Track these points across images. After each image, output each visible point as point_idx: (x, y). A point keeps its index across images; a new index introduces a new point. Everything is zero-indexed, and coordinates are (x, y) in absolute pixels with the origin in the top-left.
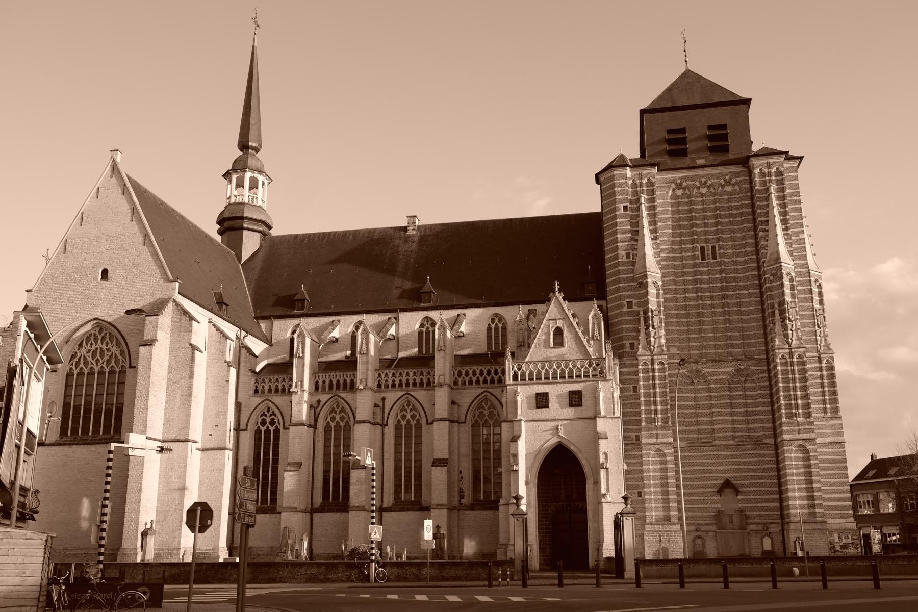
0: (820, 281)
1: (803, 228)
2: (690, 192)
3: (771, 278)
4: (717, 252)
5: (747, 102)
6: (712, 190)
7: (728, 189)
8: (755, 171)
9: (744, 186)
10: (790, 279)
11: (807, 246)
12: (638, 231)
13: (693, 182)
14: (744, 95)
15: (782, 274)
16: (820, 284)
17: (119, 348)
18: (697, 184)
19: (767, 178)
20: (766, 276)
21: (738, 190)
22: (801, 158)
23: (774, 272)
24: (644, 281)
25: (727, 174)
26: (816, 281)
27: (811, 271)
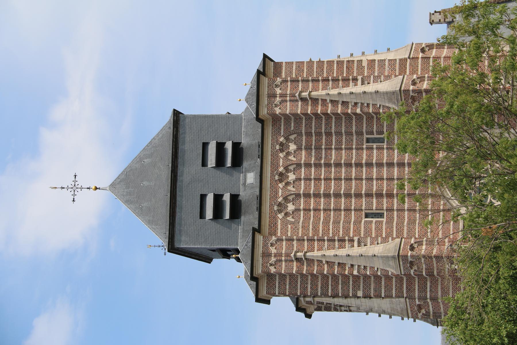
0: (423, 46)
1: (353, 61)
2: (293, 164)
3: (415, 267)
4: (375, 136)
5: (176, 114)
6: (291, 168)
7: (292, 147)
8: (272, 272)
9: (292, 129)
10: (419, 245)
11: (377, 57)
12: (339, 263)
13: (279, 221)
14: (168, 116)
15: (413, 91)
16: (427, 46)
17: (488, 294)
18: (280, 216)
19: (283, 258)
20: (412, 274)
21: (295, 135)
23: (410, 101)
24: (411, 94)
25: (273, 146)
26: (423, 50)
27: (411, 57)
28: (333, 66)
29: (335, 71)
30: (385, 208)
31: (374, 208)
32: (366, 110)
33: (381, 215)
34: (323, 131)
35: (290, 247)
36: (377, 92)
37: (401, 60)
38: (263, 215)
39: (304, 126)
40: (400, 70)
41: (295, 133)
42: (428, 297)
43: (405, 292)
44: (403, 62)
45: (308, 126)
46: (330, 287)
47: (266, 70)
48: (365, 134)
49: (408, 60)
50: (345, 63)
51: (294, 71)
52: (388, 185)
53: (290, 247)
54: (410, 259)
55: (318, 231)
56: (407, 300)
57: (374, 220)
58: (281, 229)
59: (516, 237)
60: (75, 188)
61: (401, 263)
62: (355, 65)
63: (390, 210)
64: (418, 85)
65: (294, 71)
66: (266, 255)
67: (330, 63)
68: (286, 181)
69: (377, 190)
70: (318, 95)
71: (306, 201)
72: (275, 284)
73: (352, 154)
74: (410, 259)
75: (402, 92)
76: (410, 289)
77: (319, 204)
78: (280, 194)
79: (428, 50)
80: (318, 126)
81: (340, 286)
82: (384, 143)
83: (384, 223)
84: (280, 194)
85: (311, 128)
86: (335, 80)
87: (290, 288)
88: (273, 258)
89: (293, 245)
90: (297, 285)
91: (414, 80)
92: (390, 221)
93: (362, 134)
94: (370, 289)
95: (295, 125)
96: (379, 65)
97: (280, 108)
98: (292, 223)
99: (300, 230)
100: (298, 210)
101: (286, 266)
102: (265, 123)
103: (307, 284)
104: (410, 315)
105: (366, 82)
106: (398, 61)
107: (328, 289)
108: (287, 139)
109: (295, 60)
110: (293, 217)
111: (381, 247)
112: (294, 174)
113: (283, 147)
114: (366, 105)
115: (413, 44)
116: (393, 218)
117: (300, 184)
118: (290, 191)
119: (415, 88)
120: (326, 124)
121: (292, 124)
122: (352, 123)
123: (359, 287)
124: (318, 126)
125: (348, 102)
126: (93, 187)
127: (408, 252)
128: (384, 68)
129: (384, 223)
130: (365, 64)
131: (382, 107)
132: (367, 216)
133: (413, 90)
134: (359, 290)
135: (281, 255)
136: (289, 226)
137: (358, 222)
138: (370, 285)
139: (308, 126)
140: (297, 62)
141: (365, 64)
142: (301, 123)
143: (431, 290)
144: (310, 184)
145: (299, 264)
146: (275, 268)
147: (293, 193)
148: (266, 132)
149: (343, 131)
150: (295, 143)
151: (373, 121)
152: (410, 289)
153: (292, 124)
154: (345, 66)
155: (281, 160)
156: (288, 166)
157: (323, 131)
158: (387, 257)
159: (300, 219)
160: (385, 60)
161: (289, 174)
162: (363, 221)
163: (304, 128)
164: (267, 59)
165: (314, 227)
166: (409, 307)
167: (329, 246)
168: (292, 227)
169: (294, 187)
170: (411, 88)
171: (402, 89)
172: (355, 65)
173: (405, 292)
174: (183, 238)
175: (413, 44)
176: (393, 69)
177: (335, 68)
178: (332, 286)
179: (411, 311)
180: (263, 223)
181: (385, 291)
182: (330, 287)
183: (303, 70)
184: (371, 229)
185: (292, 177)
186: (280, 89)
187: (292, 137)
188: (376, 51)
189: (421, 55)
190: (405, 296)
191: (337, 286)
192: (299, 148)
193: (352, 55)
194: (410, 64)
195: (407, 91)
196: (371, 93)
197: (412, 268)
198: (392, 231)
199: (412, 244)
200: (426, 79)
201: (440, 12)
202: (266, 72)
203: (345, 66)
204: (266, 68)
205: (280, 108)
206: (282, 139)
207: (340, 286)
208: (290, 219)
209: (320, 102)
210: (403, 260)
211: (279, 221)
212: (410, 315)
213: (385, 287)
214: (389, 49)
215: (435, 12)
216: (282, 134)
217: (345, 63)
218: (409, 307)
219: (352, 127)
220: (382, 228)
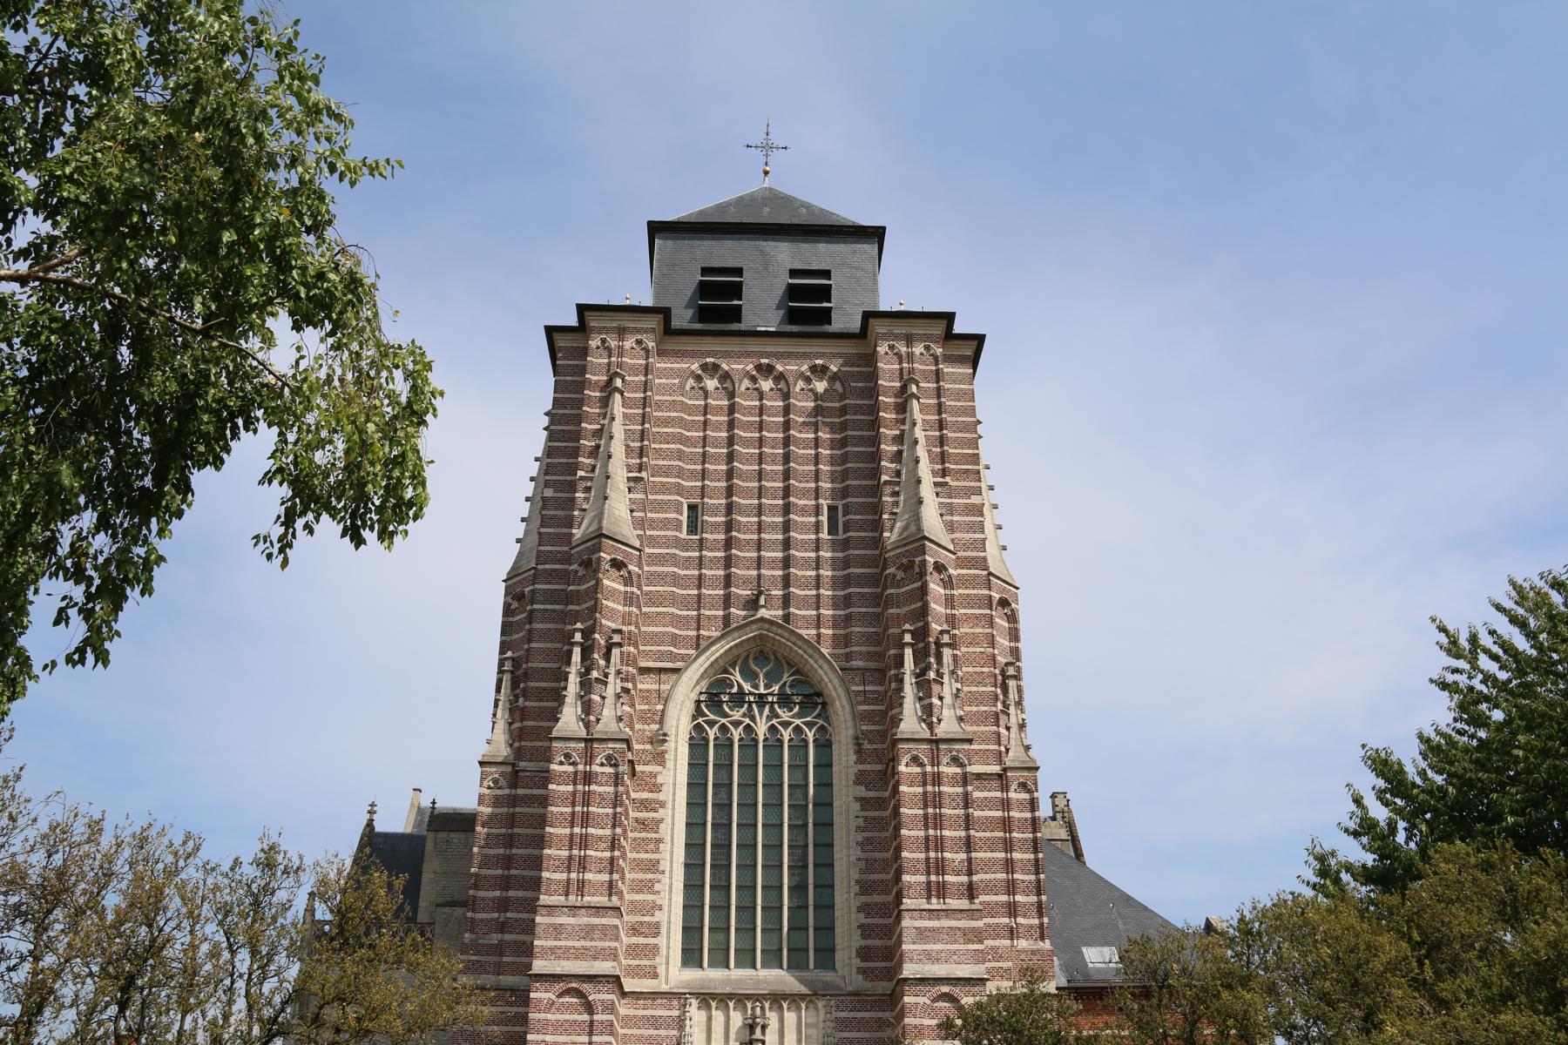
0: (1013, 605)
3: (900, 575)
4: (841, 520)
8: (590, 342)
9: (852, 384)
13: (687, 366)
15: (924, 562)
22: (979, 339)
23: (905, 561)
24: (917, 560)
28: (969, 448)
29: (960, 451)
30: (705, 535)
31: (705, 518)
32: (888, 490)
33: (692, 529)
34: (850, 433)
35: (634, 370)
36: (920, 502)
37: (985, 559)
38: (697, 339)
39: (859, 402)
40: (966, 558)
41: (844, 388)
42: (535, 606)
43: (547, 566)
44: (982, 563)
45: (858, 409)
46: (564, 444)
47: (957, 342)
48: (844, 502)
49: (986, 572)
50: (976, 467)
51: (957, 386)
52: (748, 541)
53: (634, 370)
54: (594, 557)
55: (666, 426)
56: (533, 572)
57: (684, 518)
58: (671, 369)
59: (38, 2)
60: (767, 148)
61: (589, 544)
62: (972, 484)
63: (701, 545)
64: (935, 574)
65: (957, 386)
66: (621, 333)
67: (972, 411)
68: (758, 376)
69: (740, 522)
70: (912, 410)
71: (721, 408)
72: (574, 359)
73: (808, 482)
74: (594, 557)
75: (922, 543)
76: (550, 576)
77: (717, 428)
78: (734, 366)
79: (1006, 614)
80: (857, 425)
81: (564, 461)
82: (829, 534)
83: (678, 534)
84: (734, 366)
85: (854, 414)
86: (942, 441)
87: (567, 381)
88: (616, 343)
89: (637, 375)
90: (570, 392)
91: (946, 570)
92: (685, 545)
93: (844, 497)
94: (556, 509)
95: (860, 388)
96: (974, 523)
97: (887, 353)
98: (682, 386)
99: (669, 398)
100: (706, 394)
101: (600, 364)
102: (861, 341)
103: (572, 408)
104: (510, 582)
105: (939, 489)
106: (982, 554)
107: (559, 441)
108: (834, 378)
109: (977, 404)
110: (693, 388)
111: (623, 515)
112: (772, 390)
113: (820, 371)
114: (897, 489)
115: (1017, 588)
116: (687, 550)
117: (752, 400)
118: (741, 382)
119: (930, 569)
120: (862, 438)
121: (860, 385)
122: (864, 479)
123: (561, 491)
124: (857, 425)
125: (900, 462)
126: (768, 169)
127: (609, 554)
128: (968, 532)
129: (678, 534)
130: (975, 499)
131: (894, 517)
132: (692, 508)
133: (925, 560)
134: (555, 492)
135: (621, 355)
136: (677, 381)
137: (679, 490)
138: (563, 509)
139: (858, 409)
140: (973, 391)
141: (975, 499)
142: (864, 399)
143: (547, 610)
144: (752, 415)
145: (602, 384)
146: (598, 348)
147: (737, 386)
148: (845, 342)
149: (849, 465)
150: (826, 390)
151: (868, 513)
152: (550, 576)
153: (860, 385)
154: (970, 467)
155: (796, 368)
156: (787, 381)
157: (850, 433)
158: (600, 521)
159: (690, 399)
160: (982, 515)
161: (770, 381)
162: (682, 500)
163: (853, 402)
164: (975, 343)
165: (673, 420)
166: (521, 577)
167: (633, 432)
168: (674, 385)
169: (748, 389)
170: (930, 560)
171: (927, 543)
172: (972, 484)
173: (547, 566)
174: (670, 243)
175: (1017, 588)
176: (968, 546)
177: (965, 451)
178: (566, 447)
179: (515, 583)
180: (684, 339)
181: (550, 534)
182: (564, 444)
183: (959, 400)
184: (666, 512)
185: (766, 385)
186: (922, 354)
187: (838, 386)
188: (1004, 548)
189: (996, 596)
190: (540, 567)
191: (564, 456)
192: (817, 397)
193: (991, 488)
194: (978, 576)
195: (922, 551)
196: (918, 493)
197: (580, 565)
198: (660, 547)
199: (626, 566)
200: (948, 592)
201: (1068, 805)
202: (952, 342)
203: (970, 467)
204: (961, 342)
205: (887, 353)
206: (834, 368)
207: (564, 461)
208: (691, 382)
209: (901, 417)
210: (594, 545)
211: (687, 366)
212: (510, 582)
213: (557, 534)
214: (1004, 548)
215: (1068, 801)
216: (843, 369)
217: (976, 467)
218: (521, 577)
219: (856, 479)
220: (668, 529)
